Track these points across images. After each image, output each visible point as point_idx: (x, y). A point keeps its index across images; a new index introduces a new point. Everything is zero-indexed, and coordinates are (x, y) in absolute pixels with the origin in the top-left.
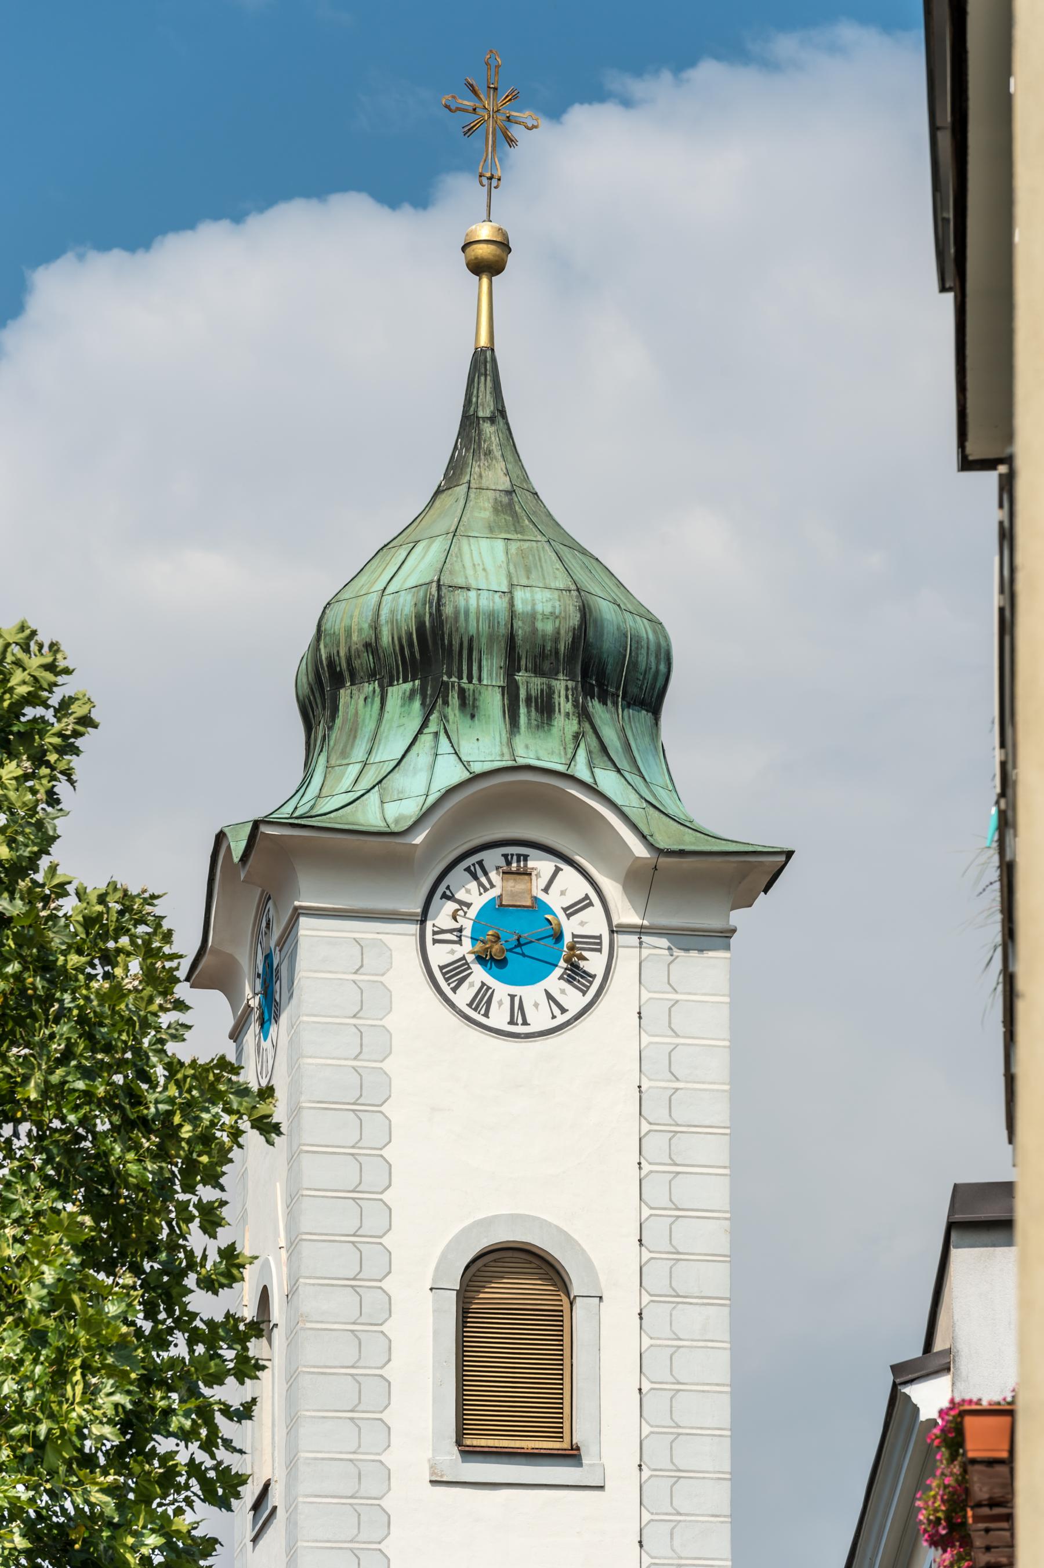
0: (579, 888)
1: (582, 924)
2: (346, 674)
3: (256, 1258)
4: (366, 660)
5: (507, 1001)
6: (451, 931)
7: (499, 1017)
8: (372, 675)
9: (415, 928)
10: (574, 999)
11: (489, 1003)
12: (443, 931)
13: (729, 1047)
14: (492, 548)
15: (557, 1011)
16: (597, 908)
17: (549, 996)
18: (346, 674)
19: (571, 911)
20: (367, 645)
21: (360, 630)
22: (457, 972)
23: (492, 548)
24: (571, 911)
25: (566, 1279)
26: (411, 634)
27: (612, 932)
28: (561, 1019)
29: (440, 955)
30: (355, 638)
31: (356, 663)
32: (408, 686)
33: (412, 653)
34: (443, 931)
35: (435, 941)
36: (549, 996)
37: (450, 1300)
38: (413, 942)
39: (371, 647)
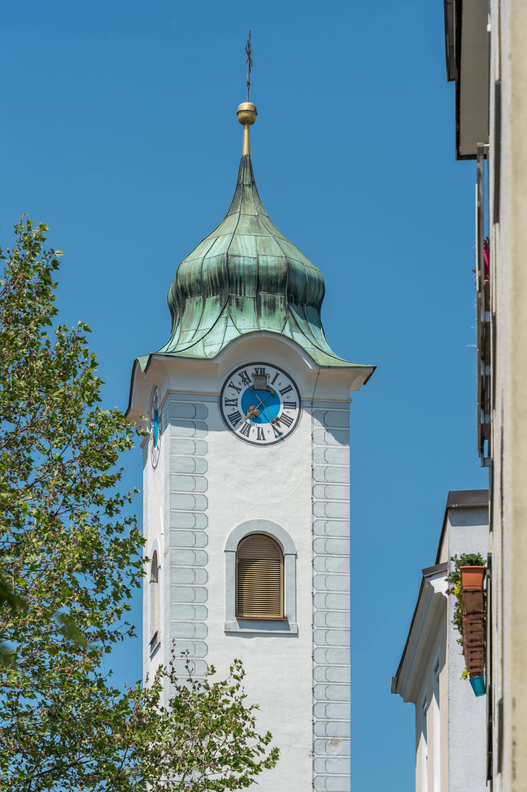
5: (256, 430)
6: (233, 400)
8: (199, 293)
12: (229, 401)
20: (197, 280)
21: (195, 274)
24: (283, 392)
26: (216, 280)
30: (192, 277)
31: (193, 288)
32: (215, 297)
33: (216, 284)
39: (200, 282)
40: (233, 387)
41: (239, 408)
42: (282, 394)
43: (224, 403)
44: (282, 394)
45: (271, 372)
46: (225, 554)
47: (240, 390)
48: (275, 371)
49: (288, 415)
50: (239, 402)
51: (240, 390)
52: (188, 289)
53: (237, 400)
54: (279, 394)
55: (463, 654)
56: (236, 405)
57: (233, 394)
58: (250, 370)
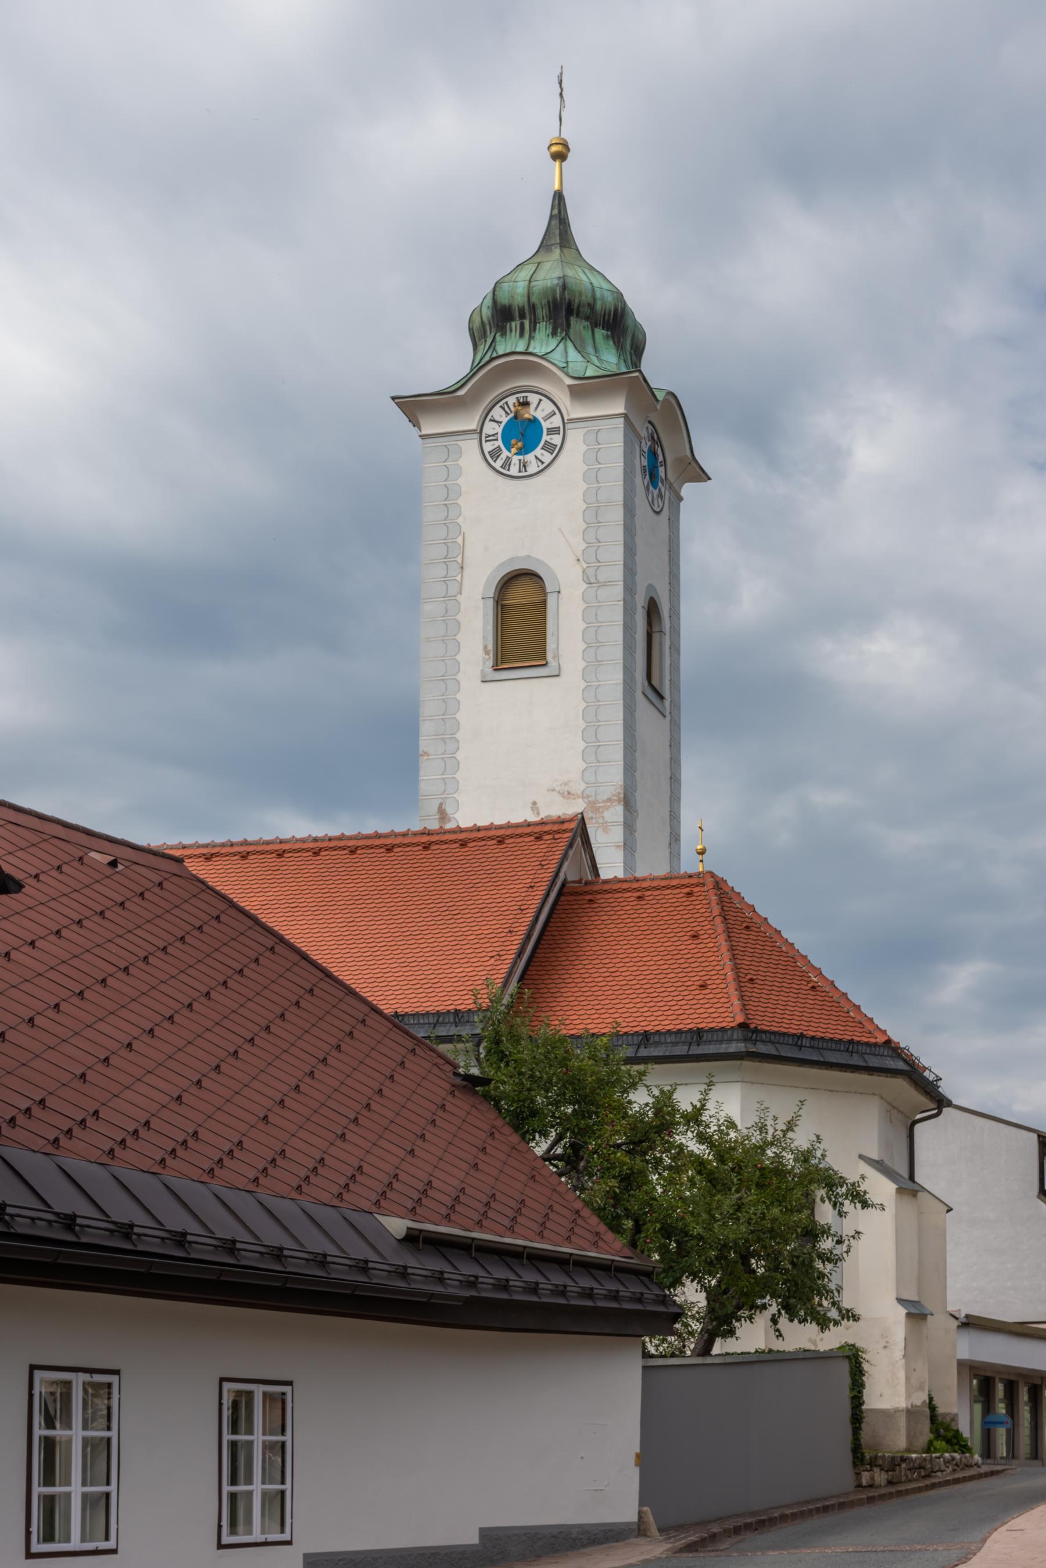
0: (547, 407)
1: (551, 423)
2: (575, 311)
3: (534, 803)
4: (586, 310)
5: (517, 463)
6: (493, 435)
7: (514, 471)
8: (587, 318)
9: (477, 436)
10: (547, 458)
11: (510, 465)
12: (489, 436)
13: (626, 416)
14: (957, 1318)
15: (540, 464)
16: (558, 415)
17: (537, 458)
18: (575, 311)
19: (546, 419)
20: (589, 305)
21: (586, 296)
22: (495, 454)
23: (957, 1318)
24: (546, 419)
25: (515, 573)
26: (609, 315)
27: (564, 423)
28: (542, 467)
29: (488, 447)
30: (583, 298)
31: (582, 309)
33: (609, 319)
34: (489, 436)
35: (486, 441)
36: (537, 458)
37: (490, 603)
38: (476, 442)
40: (494, 421)
41: (500, 443)
42: (545, 421)
43: (501, 404)
44: (545, 421)
45: (533, 399)
46: (482, 601)
47: (501, 423)
48: (537, 397)
49: (552, 442)
50: (499, 436)
51: (501, 423)
52: (575, 307)
53: (497, 434)
54: (542, 421)
55: (766, 919)
56: (497, 440)
57: (501, 416)
58: (512, 400)
